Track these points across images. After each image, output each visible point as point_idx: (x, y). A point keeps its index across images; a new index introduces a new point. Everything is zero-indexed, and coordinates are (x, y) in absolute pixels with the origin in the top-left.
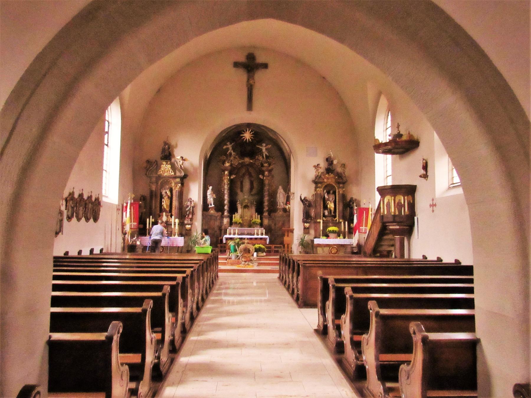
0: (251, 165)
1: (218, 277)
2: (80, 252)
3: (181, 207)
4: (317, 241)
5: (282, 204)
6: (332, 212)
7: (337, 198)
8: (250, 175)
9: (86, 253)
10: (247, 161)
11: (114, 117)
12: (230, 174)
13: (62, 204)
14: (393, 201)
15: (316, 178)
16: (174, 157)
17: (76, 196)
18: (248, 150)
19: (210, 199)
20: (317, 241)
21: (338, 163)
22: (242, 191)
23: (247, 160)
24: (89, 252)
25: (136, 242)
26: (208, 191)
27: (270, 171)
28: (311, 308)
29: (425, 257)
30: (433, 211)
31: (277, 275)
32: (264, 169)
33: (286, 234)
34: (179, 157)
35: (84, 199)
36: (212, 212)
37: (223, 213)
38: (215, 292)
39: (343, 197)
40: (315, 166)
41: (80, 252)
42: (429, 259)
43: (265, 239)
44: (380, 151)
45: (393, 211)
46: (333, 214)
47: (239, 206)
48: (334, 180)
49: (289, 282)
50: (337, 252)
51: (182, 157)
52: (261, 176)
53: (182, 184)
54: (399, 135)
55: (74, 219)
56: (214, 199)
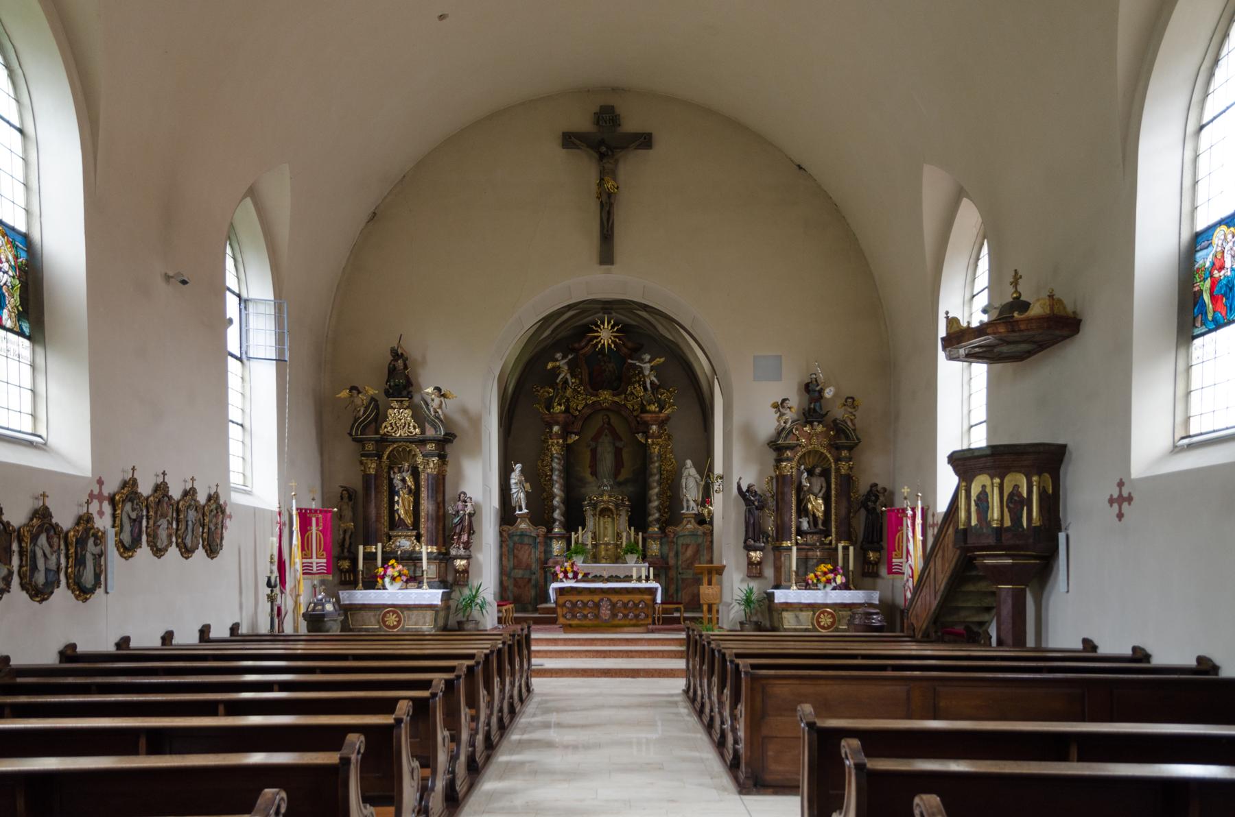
0: (617, 409)
1: (529, 690)
2: (167, 637)
3: (441, 517)
4: (780, 596)
5: (692, 504)
6: (820, 522)
7: (833, 486)
8: (616, 436)
9: (187, 637)
10: (605, 400)
11: (249, 283)
12: (565, 433)
13: (101, 513)
14: (996, 491)
15: (779, 433)
16: (420, 389)
17: (145, 489)
18: (609, 372)
19: (519, 495)
20: (780, 596)
21: (836, 395)
22: (594, 473)
23: (606, 396)
24: (197, 635)
25: (323, 605)
26: (513, 475)
27: (662, 424)
28: (775, 793)
29: (1089, 645)
30: (1120, 516)
31: (681, 683)
32: (647, 417)
33: (705, 580)
34: (430, 390)
35: (170, 498)
36: (523, 526)
37: (550, 530)
38: (515, 737)
39: (848, 482)
40: (776, 406)
41: (167, 637)
42: (1103, 650)
43: (652, 591)
44: (962, 352)
45: (996, 515)
46: (820, 527)
47: (589, 512)
48: (826, 442)
49: (712, 710)
50: (833, 623)
51: (438, 389)
52: (640, 436)
53: (442, 457)
54: (1019, 304)
55: (144, 552)
56: (527, 495)
